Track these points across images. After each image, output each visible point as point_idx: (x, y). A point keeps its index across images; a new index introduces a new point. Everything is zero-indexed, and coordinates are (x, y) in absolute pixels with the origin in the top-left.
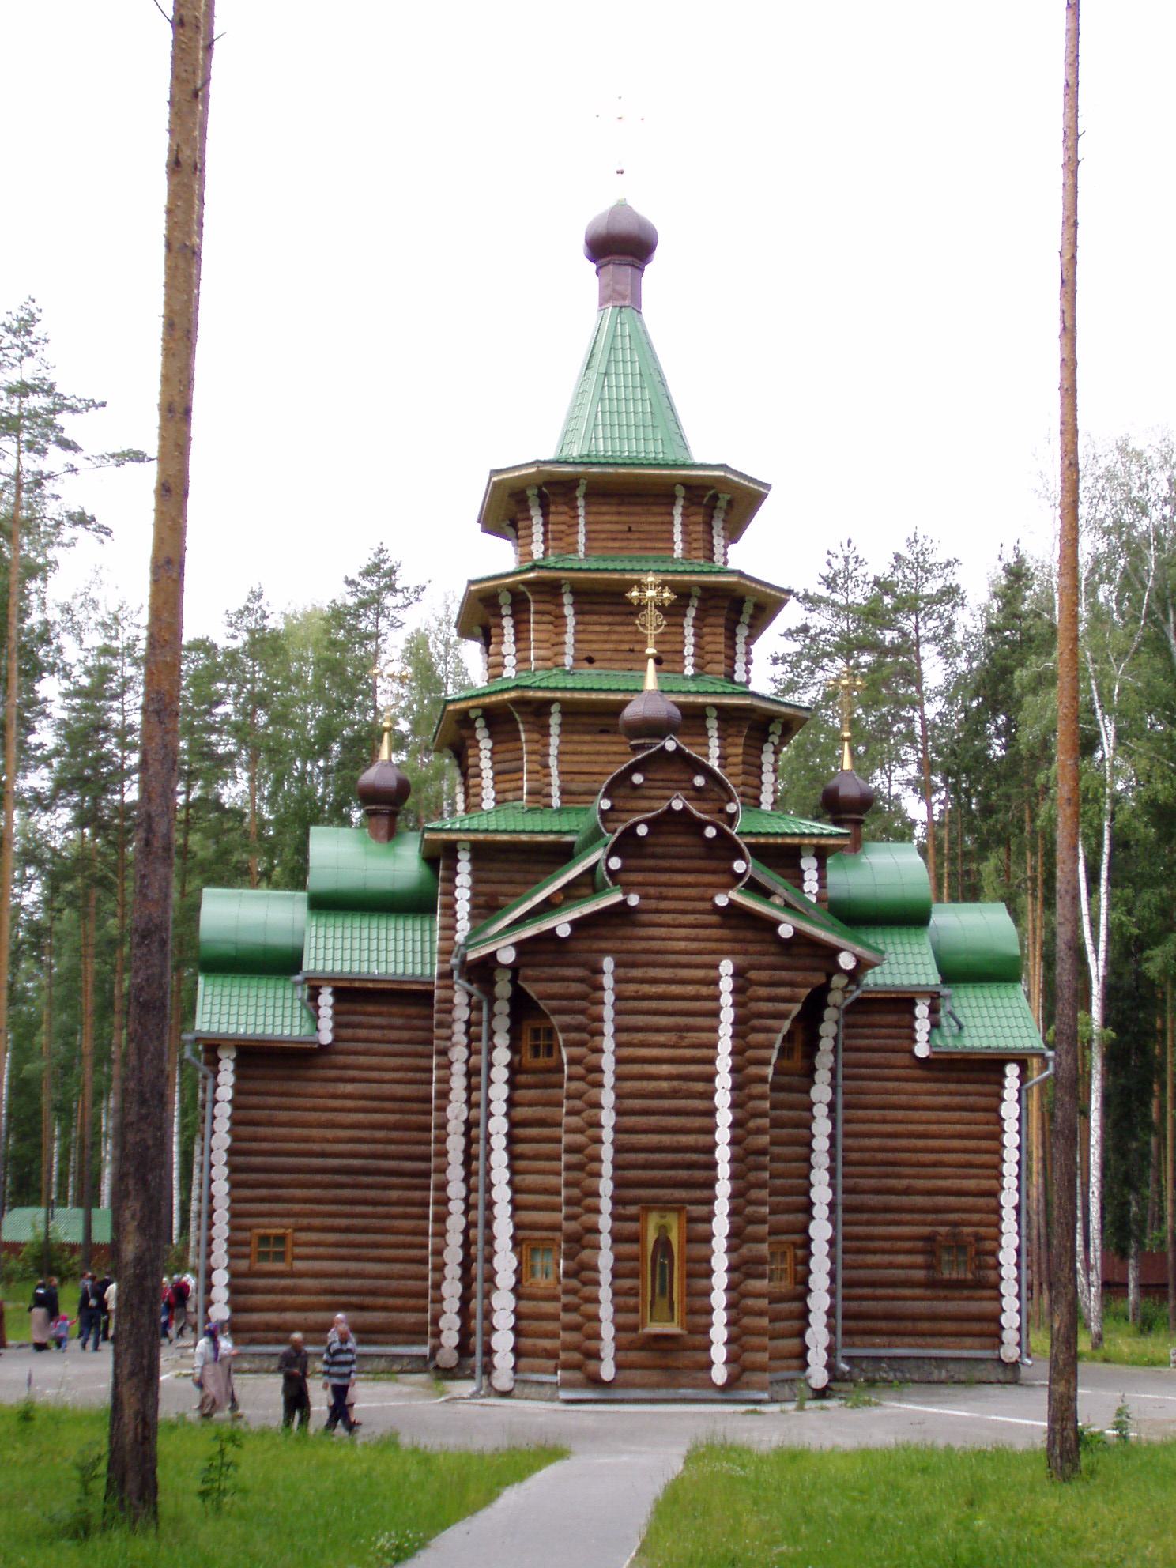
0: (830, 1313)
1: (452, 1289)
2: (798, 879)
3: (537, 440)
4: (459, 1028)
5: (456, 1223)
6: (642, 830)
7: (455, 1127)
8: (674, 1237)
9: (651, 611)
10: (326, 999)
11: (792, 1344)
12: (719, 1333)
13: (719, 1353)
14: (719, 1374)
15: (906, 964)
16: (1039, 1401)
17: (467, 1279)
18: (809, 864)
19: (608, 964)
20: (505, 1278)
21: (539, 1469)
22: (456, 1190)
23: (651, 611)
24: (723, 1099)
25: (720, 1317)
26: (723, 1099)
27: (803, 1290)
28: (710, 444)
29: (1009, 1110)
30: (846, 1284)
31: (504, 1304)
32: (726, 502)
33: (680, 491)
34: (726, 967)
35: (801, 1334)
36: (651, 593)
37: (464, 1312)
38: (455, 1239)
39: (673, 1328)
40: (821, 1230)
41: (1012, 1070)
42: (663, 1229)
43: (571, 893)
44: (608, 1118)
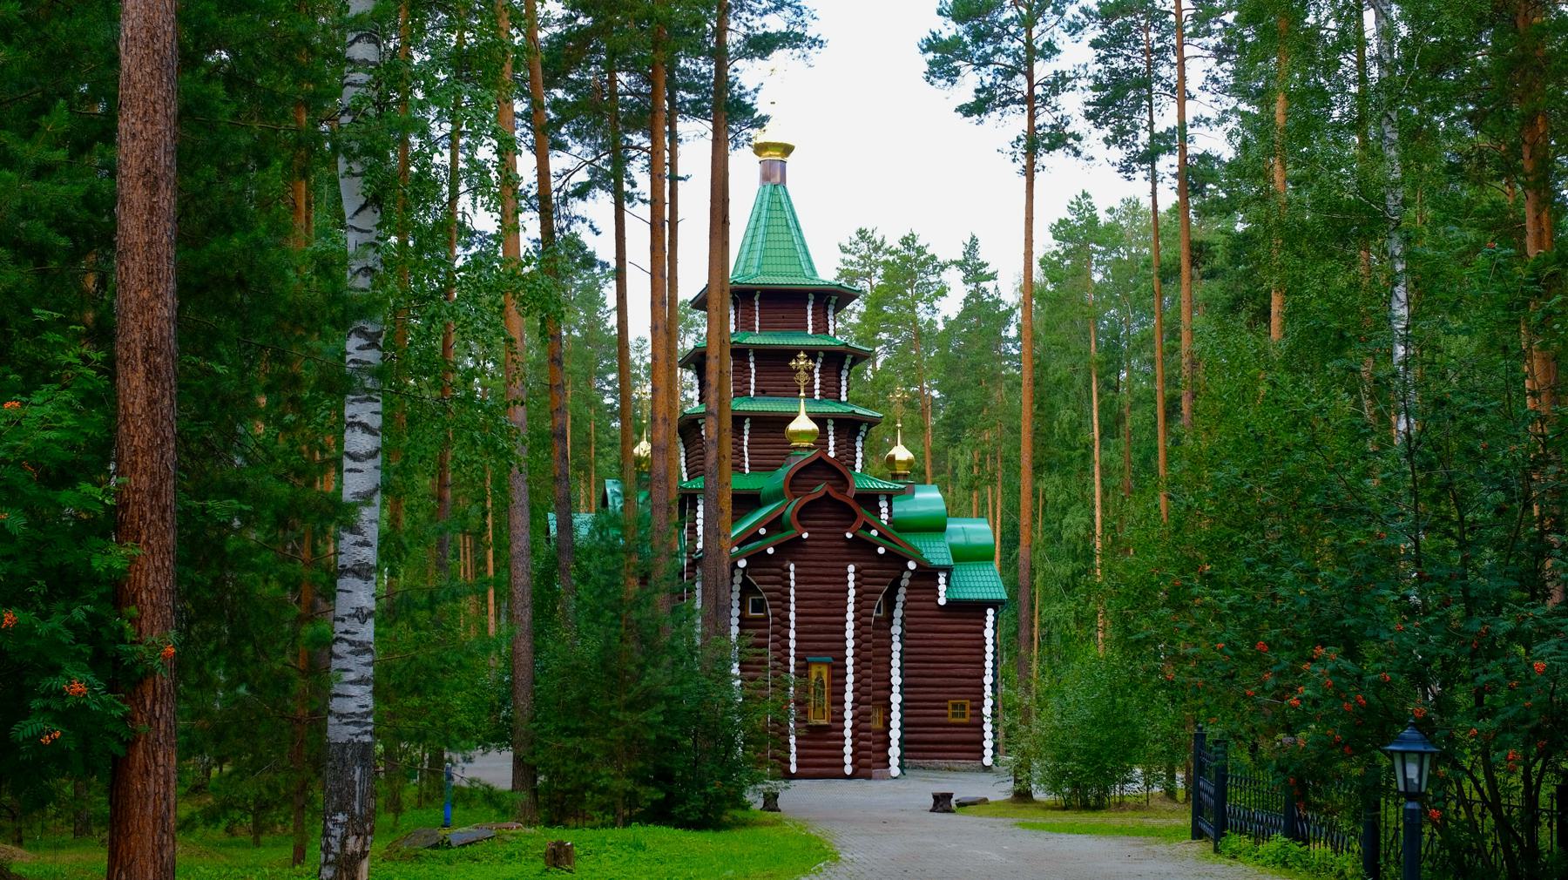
2: (877, 511)
6: (771, 551)
8: (825, 677)
9: (802, 373)
11: (882, 756)
14: (848, 770)
15: (936, 552)
18: (883, 504)
23: (802, 373)
29: (989, 633)
30: (903, 742)
33: (811, 297)
34: (851, 568)
35: (886, 751)
39: (824, 722)
40: (896, 699)
41: (990, 612)
42: (820, 674)
44: (792, 644)
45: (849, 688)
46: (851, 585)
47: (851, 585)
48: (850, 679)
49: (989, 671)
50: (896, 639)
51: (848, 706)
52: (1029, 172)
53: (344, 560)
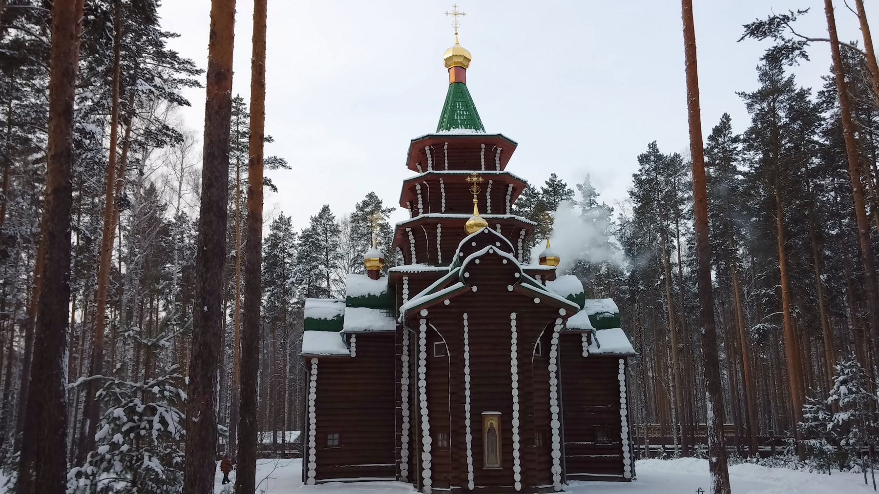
0: (561, 459)
1: (405, 453)
4: (405, 348)
5: (406, 426)
7: (405, 388)
10: (353, 340)
12: (517, 469)
13: (517, 477)
15: (580, 321)
17: (411, 449)
19: (465, 316)
20: (427, 448)
21: (205, 148)
22: (406, 413)
24: (514, 370)
25: (517, 462)
26: (514, 370)
27: (428, 345)
28: (492, 124)
31: (426, 457)
32: (502, 147)
34: (513, 316)
36: (474, 179)
37: (410, 462)
38: (405, 432)
40: (555, 424)
41: (621, 361)
45: (516, 414)
46: (514, 329)
47: (514, 329)
49: (623, 406)
50: (553, 375)
51: (515, 430)
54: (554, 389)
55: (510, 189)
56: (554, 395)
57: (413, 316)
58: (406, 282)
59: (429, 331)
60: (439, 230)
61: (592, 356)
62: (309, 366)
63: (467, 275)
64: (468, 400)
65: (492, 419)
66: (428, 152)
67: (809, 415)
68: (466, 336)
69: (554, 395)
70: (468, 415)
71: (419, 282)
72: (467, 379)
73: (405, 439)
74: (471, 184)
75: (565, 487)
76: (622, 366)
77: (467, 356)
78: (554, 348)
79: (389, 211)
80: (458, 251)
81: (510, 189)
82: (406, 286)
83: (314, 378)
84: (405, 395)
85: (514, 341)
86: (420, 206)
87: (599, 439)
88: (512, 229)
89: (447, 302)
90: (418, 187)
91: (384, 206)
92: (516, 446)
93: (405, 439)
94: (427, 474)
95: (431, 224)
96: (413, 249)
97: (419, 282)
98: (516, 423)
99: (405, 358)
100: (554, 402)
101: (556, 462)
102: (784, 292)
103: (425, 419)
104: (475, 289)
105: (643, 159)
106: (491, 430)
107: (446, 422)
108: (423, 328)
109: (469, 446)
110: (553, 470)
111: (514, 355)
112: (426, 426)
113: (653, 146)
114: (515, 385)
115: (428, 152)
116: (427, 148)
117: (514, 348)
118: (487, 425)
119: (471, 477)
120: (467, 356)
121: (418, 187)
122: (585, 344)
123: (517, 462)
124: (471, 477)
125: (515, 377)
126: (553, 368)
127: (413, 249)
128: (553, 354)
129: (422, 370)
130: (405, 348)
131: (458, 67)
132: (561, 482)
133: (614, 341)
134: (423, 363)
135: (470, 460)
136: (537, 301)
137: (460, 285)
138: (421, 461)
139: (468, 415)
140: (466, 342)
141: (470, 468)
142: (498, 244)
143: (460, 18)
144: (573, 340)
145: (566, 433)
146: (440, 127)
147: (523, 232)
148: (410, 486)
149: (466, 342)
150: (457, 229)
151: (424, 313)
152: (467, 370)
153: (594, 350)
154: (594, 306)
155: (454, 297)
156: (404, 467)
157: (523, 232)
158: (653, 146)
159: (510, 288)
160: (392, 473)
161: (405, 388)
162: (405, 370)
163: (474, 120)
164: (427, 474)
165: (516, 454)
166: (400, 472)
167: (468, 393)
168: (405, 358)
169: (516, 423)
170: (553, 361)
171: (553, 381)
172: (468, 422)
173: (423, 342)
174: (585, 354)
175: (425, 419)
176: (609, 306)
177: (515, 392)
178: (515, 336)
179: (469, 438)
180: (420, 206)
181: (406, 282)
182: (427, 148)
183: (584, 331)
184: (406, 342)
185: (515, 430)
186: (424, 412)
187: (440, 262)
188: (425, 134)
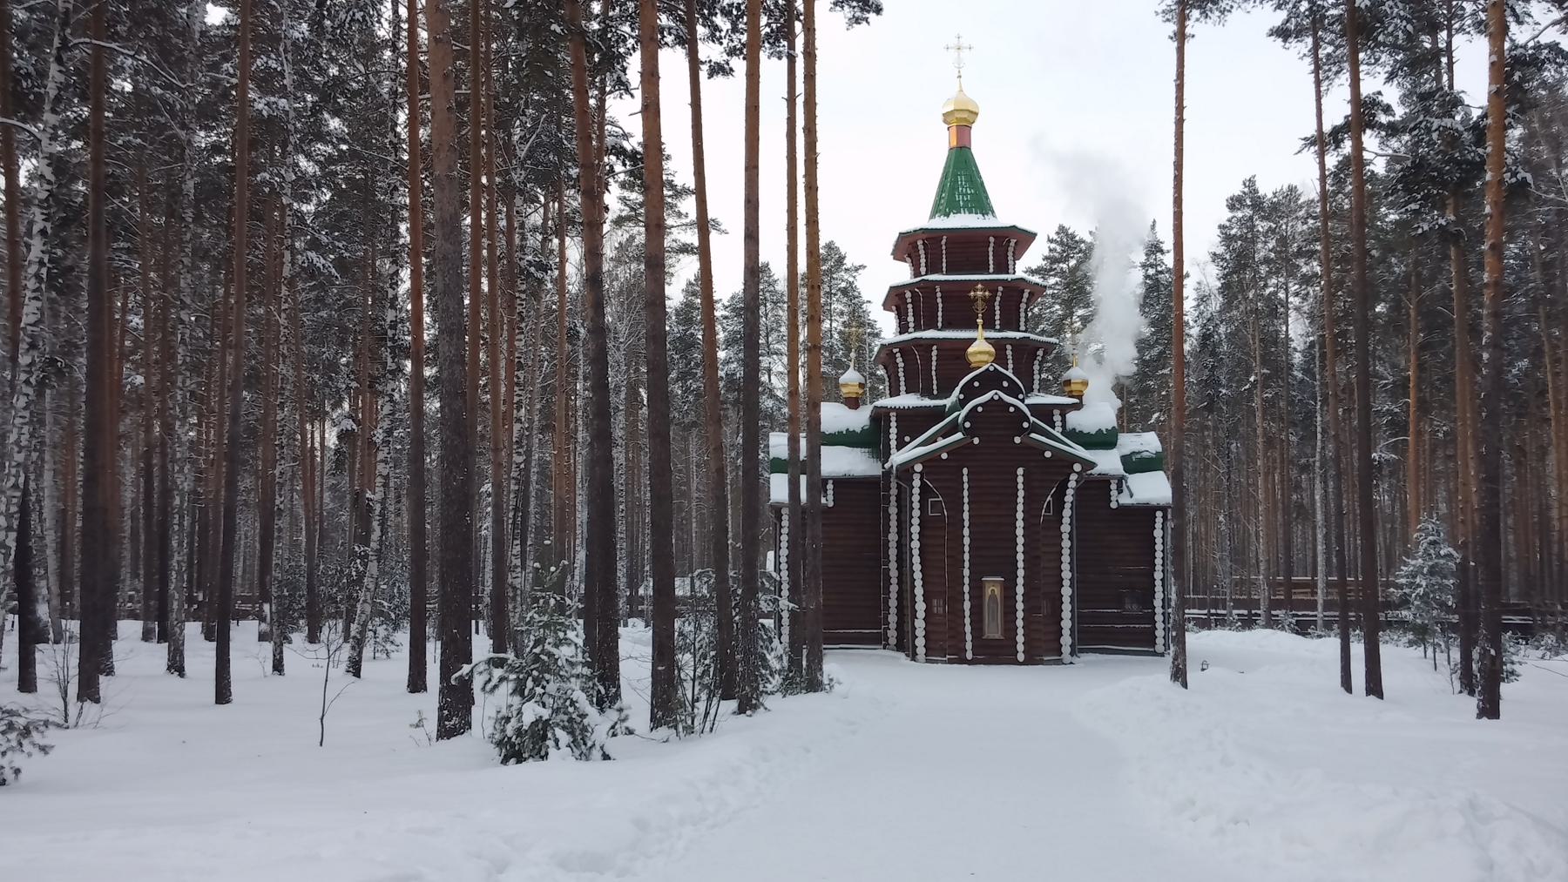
1: (893, 619)
3: (919, 216)
4: (893, 499)
5: (894, 588)
7: (893, 545)
12: (1020, 639)
14: (1021, 657)
15: (1107, 462)
16: (702, 56)
18: (1057, 418)
19: (965, 471)
20: (921, 614)
22: (894, 573)
24: (1020, 532)
25: (1020, 631)
26: (1020, 532)
30: (1078, 618)
31: (920, 624)
34: (1020, 471)
38: (894, 595)
40: (1066, 591)
41: (1159, 514)
43: (945, 433)
45: (1020, 581)
46: (1020, 486)
47: (1020, 486)
48: (1021, 573)
49: (1159, 568)
50: (1065, 536)
51: (1019, 598)
52: (1181, 37)
53: (567, 239)
54: (1066, 552)
55: (1026, 295)
56: (1066, 558)
57: (906, 470)
58: (893, 419)
59: (923, 487)
60: (934, 353)
61: (1123, 509)
62: (779, 518)
63: (968, 425)
64: (967, 564)
65: (993, 586)
66: (921, 247)
67: (1403, 581)
68: (966, 493)
69: (1066, 558)
70: (966, 581)
71: (913, 423)
72: (967, 541)
73: (893, 603)
74: (975, 299)
75: (1075, 659)
76: (1159, 520)
77: (966, 516)
78: (1068, 506)
79: (857, 270)
80: (958, 389)
81: (1026, 295)
82: (893, 424)
83: (785, 531)
84: (893, 553)
85: (1020, 500)
86: (911, 319)
87: (1128, 606)
88: (1026, 353)
89: (944, 456)
90: (908, 295)
91: (848, 263)
92: (1020, 615)
93: (893, 603)
94: (920, 642)
95: (926, 345)
96: (901, 374)
97: (913, 423)
98: (1020, 590)
99: (893, 510)
100: (1066, 567)
101: (1066, 632)
102: (1412, 410)
103: (918, 583)
104: (976, 441)
105: (1234, 203)
106: (993, 596)
107: (942, 586)
108: (917, 483)
109: (967, 613)
110: (1062, 641)
111: (1020, 515)
112: (919, 591)
113: (1250, 183)
114: (1020, 548)
115: (921, 247)
116: (920, 243)
117: (1020, 507)
118: (988, 592)
119: (969, 646)
120: (966, 516)
121: (908, 295)
122: (1114, 493)
123: (1020, 631)
124: (969, 646)
125: (1020, 540)
126: (1066, 528)
127: (901, 374)
128: (1067, 513)
129: (915, 529)
130: (893, 499)
131: (961, 123)
132: (1072, 654)
133: (1152, 488)
134: (916, 521)
135: (968, 629)
136: (1048, 454)
137: (959, 436)
138: (914, 628)
139: (966, 581)
140: (966, 500)
141: (969, 637)
142: (1005, 384)
143: (965, 53)
144: (1097, 488)
145: (1079, 599)
146: (937, 210)
147: (1040, 353)
148: (902, 655)
149: (966, 500)
150: (956, 354)
151: (918, 468)
152: (966, 532)
153: (1125, 500)
154: (1131, 442)
155: (952, 450)
156: (892, 634)
157: (1040, 353)
158: (1250, 183)
159: (1017, 440)
160: (879, 640)
161: (893, 545)
162: (893, 523)
163: (981, 204)
164: (920, 642)
165: (1020, 623)
166: (887, 639)
167: (967, 557)
168: (893, 510)
169: (1020, 590)
170: (1066, 520)
171: (1066, 543)
172: (966, 589)
173: (916, 498)
174: (1114, 505)
175: (918, 583)
176: (1149, 443)
177: (1020, 557)
178: (1021, 493)
179: (967, 605)
180: (911, 319)
181: (893, 419)
182: (920, 243)
183: (1113, 477)
184: (894, 491)
185: (1019, 598)
186: (918, 575)
187: (969, 656)
188: (918, 226)
